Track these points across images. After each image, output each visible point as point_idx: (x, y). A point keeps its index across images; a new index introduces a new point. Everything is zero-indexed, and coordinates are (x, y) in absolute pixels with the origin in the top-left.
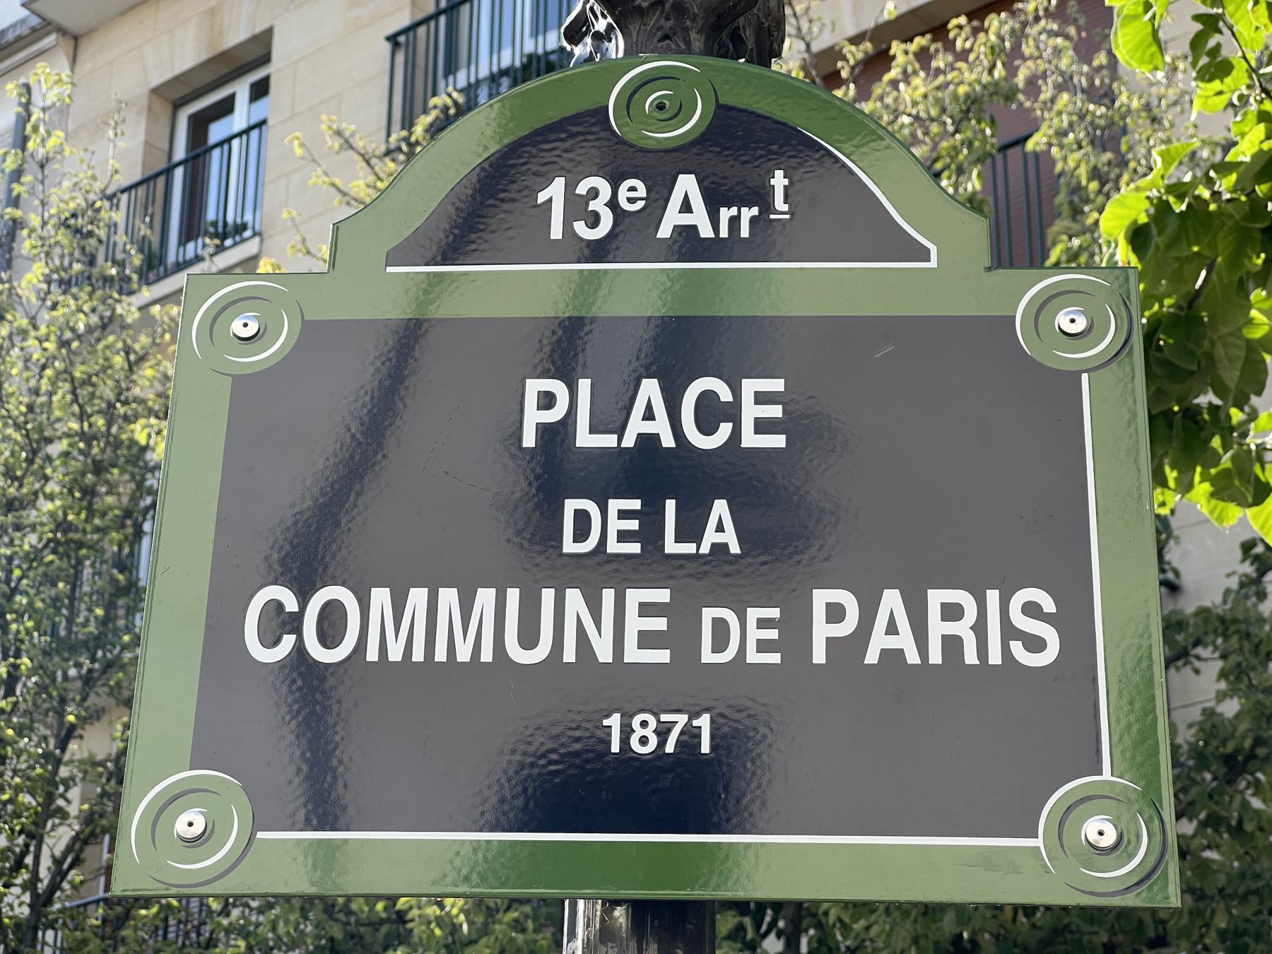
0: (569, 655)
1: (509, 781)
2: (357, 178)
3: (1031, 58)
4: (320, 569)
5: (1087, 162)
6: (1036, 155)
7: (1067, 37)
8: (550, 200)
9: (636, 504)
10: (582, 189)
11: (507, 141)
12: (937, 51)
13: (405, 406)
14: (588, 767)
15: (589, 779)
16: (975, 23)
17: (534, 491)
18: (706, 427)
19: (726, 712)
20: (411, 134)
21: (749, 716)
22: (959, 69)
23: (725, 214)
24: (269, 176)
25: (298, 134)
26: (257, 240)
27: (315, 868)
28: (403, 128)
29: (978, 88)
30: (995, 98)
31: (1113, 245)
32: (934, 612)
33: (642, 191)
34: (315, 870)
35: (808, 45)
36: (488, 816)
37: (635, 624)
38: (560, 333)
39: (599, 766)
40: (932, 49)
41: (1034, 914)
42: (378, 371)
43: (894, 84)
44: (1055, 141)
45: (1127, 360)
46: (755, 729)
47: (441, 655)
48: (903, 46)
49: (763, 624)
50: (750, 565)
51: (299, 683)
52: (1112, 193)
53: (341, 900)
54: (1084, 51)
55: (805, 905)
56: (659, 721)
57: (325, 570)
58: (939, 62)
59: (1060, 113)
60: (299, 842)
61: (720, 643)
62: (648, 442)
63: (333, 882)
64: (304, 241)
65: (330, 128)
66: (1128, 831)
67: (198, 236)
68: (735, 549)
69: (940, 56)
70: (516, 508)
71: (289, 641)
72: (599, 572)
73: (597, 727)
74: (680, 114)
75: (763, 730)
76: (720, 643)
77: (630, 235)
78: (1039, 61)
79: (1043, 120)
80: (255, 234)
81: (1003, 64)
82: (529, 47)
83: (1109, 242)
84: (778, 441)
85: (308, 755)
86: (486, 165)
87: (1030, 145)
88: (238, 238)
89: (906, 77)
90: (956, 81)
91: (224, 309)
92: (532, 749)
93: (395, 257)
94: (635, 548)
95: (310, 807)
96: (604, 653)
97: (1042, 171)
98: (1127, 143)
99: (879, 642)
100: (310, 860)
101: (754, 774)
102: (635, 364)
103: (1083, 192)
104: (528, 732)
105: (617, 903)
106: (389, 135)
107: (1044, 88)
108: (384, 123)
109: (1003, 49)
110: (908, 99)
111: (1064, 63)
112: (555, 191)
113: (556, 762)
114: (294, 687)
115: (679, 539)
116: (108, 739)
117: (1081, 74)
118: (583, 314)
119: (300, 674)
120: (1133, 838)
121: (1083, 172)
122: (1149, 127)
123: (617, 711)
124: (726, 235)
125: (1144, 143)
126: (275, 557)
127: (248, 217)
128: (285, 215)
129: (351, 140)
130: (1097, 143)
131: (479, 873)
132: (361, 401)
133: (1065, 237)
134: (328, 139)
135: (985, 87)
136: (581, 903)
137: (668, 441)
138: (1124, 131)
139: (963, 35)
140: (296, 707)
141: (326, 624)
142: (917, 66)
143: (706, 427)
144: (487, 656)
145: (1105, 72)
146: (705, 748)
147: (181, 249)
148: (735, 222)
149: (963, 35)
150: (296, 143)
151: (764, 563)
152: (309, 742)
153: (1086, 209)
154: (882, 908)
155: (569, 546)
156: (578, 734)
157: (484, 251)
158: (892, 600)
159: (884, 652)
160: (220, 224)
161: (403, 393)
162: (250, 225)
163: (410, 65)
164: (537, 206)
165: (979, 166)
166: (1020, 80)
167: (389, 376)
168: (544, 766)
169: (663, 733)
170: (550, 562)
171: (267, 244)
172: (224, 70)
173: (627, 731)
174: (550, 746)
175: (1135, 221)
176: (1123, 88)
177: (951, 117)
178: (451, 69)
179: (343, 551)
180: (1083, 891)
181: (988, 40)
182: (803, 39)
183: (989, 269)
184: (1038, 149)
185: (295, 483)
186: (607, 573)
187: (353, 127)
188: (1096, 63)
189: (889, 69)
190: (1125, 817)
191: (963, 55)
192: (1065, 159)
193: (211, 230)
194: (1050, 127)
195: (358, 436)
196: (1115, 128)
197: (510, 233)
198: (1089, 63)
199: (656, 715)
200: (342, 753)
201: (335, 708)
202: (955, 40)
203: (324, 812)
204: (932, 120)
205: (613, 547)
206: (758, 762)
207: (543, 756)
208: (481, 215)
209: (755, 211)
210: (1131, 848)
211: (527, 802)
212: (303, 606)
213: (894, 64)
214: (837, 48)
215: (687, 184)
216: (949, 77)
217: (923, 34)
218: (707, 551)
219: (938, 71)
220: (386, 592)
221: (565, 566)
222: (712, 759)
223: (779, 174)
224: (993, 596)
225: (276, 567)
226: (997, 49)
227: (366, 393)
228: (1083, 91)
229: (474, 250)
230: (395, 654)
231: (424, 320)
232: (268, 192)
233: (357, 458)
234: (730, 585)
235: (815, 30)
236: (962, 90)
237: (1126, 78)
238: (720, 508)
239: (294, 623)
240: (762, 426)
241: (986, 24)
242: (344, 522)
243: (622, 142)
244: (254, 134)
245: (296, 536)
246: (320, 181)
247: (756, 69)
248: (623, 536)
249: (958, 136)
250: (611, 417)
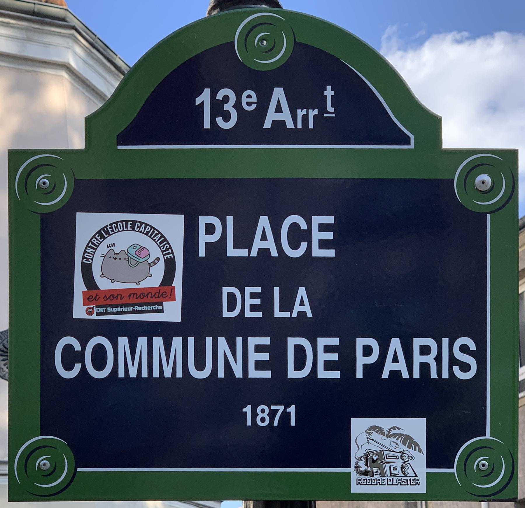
0: (221, 374)
9: (258, 290)
10: (220, 96)
18: (294, 246)
23: (300, 113)
33: (254, 99)
37: (253, 357)
47: (156, 374)
61: (299, 365)
62: (264, 252)
68: (310, 315)
71: (78, 367)
72: (243, 328)
74: (272, 50)
77: (251, 127)
96: (238, 373)
99: (389, 366)
112: (204, 98)
137: (274, 253)
143: (294, 246)
144: (179, 374)
148: (305, 118)
158: (395, 344)
159: (392, 372)
169: (272, 414)
173: (254, 415)
209: (316, 112)
212: (84, 346)
215: (279, 94)
220: (160, 339)
223: (329, 88)
224: (445, 341)
238: (302, 292)
239: (80, 357)
243: (242, 65)
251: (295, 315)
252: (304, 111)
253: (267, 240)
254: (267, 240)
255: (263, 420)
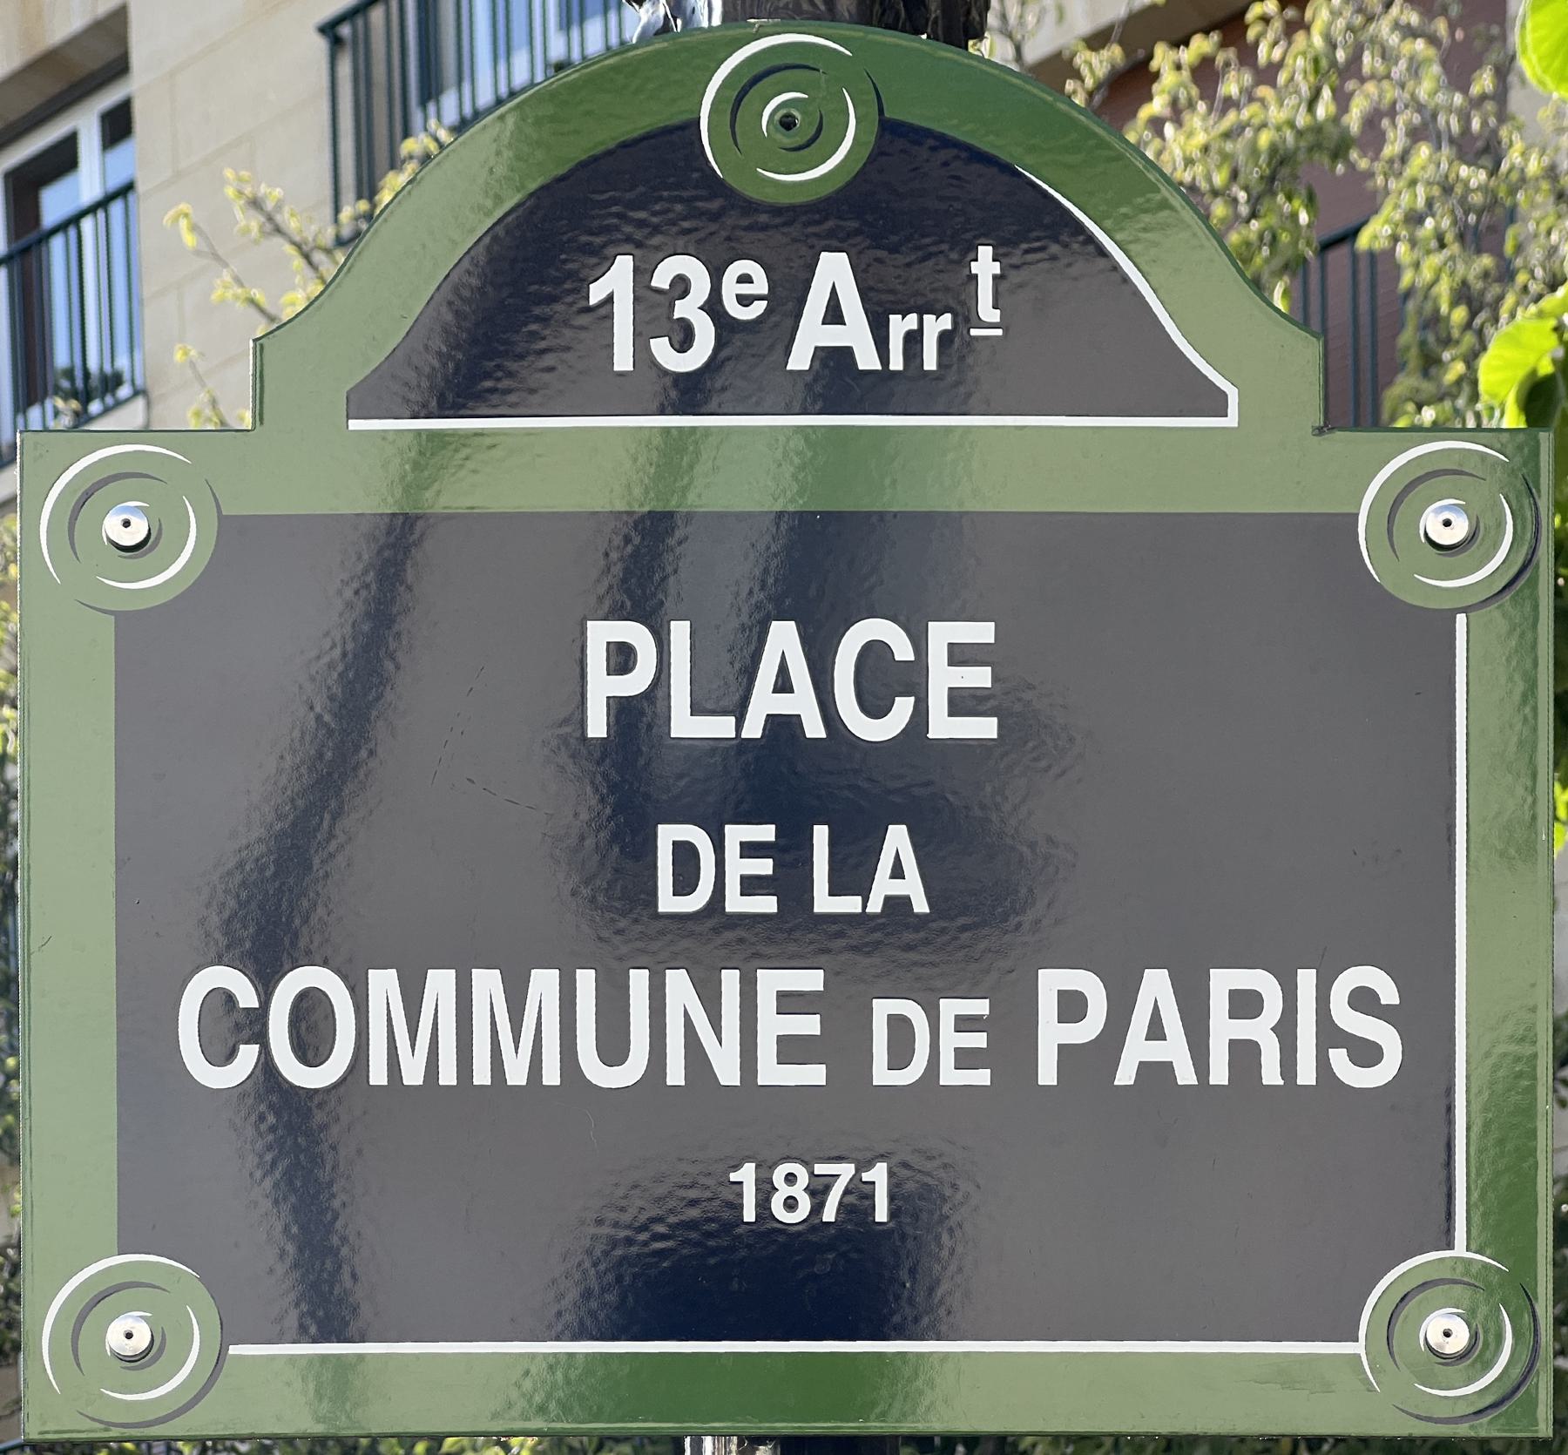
0: (676, 1074)
1: (595, 1265)
2: (293, 288)
3: (1373, 77)
4: (287, 941)
5: (1452, 274)
6: (1372, 255)
7: (1433, 40)
8: (610, 299)
10: (662, 278)
11: (533, 186)
12: (1227, 64)
13: (398, 668)
14: (711, 1243)
15: (712, 1261)
16: (1290, 13)
17: (608, 811)
18: (875, 707)
19: (909, 1158)
20: (374, 206)
21: (945, 1166)
22: (1262, 101)
23: (899, 326)
24: (148, 287)
25: (184, 207)
26: (140, 403)
27: (319, 1395)
28: (359, 197)
29: (1289, 135)
30: (1316, 156)
31: (1497, 413)
32: (1219, 1004)
33: (761, 285)
34: (320, 1400)
35: (1018, 49)
36: (568, 1317)
37: (772, 1025)
38: (637, 540)
39: (724, 1242)
40: (1220, 60)
41: (1320, 1447)
42: (349, 605)
43: (1156, 124)
44: (1404, 233)
45: (1527, 592)
46: (954, 1186)
47: (482, 1075)
48: (1172, 55)
49: (965, 1024)
50: (943, 931)
51: (271, 1119)
52: (1489, 330)
53: (364, 1442)
54: (1458, 70)
55: (1010, 1439)
56: (812, 1174)
57: (294, 944)
58: (1230, 87)
59: (1413, 183)
60: (292, 1359)
61: (899, 1058)
62: (783, 727)
63: (348, 1417)
64: (214, 403)
65: (240, 193)
66: (1486, 1332)
67: (45, 395)
68: (921, 906)
69: (1232, 74)
70: (582, 838)
71: (248, 1054)
72: (715, 942)
73: (721, 1184)
74: (815, 143)
75: (964, 1186)
76: (899, 1058)
77: (749, 355)
78: (1386, 84)
79: (1387, 192)
80: (137, 393)
81: (1334, 91)
82: (557, 51)
83: (1492, 409)
84: (985, 728)
85: (295, 1230)
86: (500, 230)
87: (1363, 241)
88: (109, 400)
89: (1177, 112)
90: (1256, 121)
91: (88, 495)
92: (626, 1218)
93: (362, 402)
94: (767, 904)
95: (304, 1307)
96: (728, 1072)
97: (1381, 291)
98: (1515, 238)
99: (1136, 1051)
100: (312, 1386)
101: (952, 1252)
102: (759, 596)
103: (1442, 325)
104: (620, 1192)
105: (759, 1440)
106: (337, 210)
107: (1390, 135)
108: (328, 191)
109: (1333, 63)
110: (1178, 152)
111: (1424, 89)
112: (615, 282)
113: (663, 1237)
114: (263, 1127)
115: (1224, 413)
116: (4, 1216)
117: (1450, 110)
118: (672, 505)
119: (271, 1106)
120: (1491, 1338)
121: (1444, 290)
122: (1551, 209)
123: (749, 1159)
124: (900, 367)
125: (1542, 239)
126: (215, 920)
127: (122, 363)
128: (178, 356)
129: (278, 218)
130: (1469, 237)
131: (559, 1401)
132: (326, 660)
133: (1411, 407)
134: (239, 215)
135: (1300, 134)
136: (708, 1442)
137: (814, 728)
138: (1512, 216)
139: (1271, 36)
140: (269, 1157)
141: (303, 1026)
142: (1195, 91)
143: (875, 707)
144: (551, 1076)
145: (1490, 106)
146: (881, 1215)
147: (20, 419)
148: (913, 340)
149: (1271, 36)
150: (183, 223)
151: (964, 929)
152: (295, 1210)
153: (1446, 356)
154: (1108, 1442)
155: (668, 902)
156: (693, 1194)
157: (508, 391)
158: (1156, 986)
159: (1144, 1067)
160: (78, 374)
161: (393, 645)
162: (126, 376)
163: (363, 79)
164: (590, 310)
165: (1286, 278)
166: (1354, 119)
167: (367, 614)
168: (645, 1244)
169: (818, 1192)
170: (639, 928)
171: (158, 410)
172: (52, 88)
173: (765, 1190)
174: (654, 1212)
175: (1534, 372)
176: (1516, 137)
177: (1246, 189)
178: (430, 91)
179: (321, 911)
180: (1418, 1417)
181: (1310, 45)
182: (1010, 36)
183: (1320, 431)
184: (1377, 246)
185: (238, 797)
186: (725, 945)
187: (278, 192)
188: (1475, 90)
189: (1150, 98)
190: (1483, 1310)
191: (1267, 75)
192: (1417, 265)
193: (65, 384)
194: (1396, 206)
195: (327, 718)
196: (1498, 211)
197: (549, 360)
198: (1465, 89)
199: (808, 1165)
200: (346, 1226)
201: (329, 1158)
202: (1256, 44)
203: (328, 1315)
204: (1215, 193)
205: (736, 903)
206: (958, 1233)
207: (644, 1228)
208: (501, 327)
209: (946, 322)
210: (1488, 1355)
211: (623, 1298)
212: (266, 993)
213: (1156, 87)
214: (1066, 54)
215: (834, 271)
216: (1246, 114)
217: (1206, 32)
218: (878, 910)
219: (1229, 103)
221: (662, 933)
222: (891, 1231)
223: (985, 252)
224: (1307, 980)
225: (217, 935)
226: (1324, 63)
227: (333, 646)
228: (1452, 141)
229: (493, 391)
230: (413, 1074)
231: (418, 517)
232: (150, 316)
233: (329, 755)
234: (915, 964)
235: (1031, 19)
236: (1264, 139)
237: (1522, 118)
238: (897, 838)
239: (254, 1026)
240: (961, 702)
241: (1308, 14)
242: (316, 861)
244: (116, 208)
245: (243, 884)
246: (229, 295)
247: (948, 52)
248: (751, 885)
249: (1255, 225)
250: (725, 688)
251: (875, 906)
252: (911, 321)
253: (792, 691)
254: (792, 691)
255: (791, 1203)
